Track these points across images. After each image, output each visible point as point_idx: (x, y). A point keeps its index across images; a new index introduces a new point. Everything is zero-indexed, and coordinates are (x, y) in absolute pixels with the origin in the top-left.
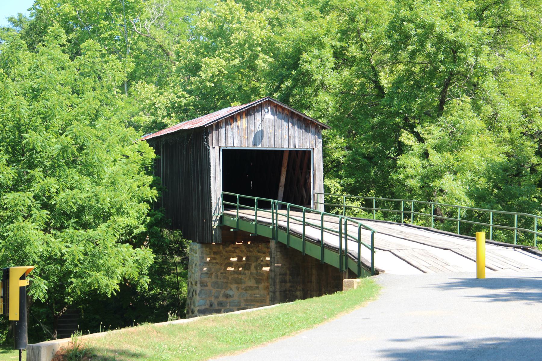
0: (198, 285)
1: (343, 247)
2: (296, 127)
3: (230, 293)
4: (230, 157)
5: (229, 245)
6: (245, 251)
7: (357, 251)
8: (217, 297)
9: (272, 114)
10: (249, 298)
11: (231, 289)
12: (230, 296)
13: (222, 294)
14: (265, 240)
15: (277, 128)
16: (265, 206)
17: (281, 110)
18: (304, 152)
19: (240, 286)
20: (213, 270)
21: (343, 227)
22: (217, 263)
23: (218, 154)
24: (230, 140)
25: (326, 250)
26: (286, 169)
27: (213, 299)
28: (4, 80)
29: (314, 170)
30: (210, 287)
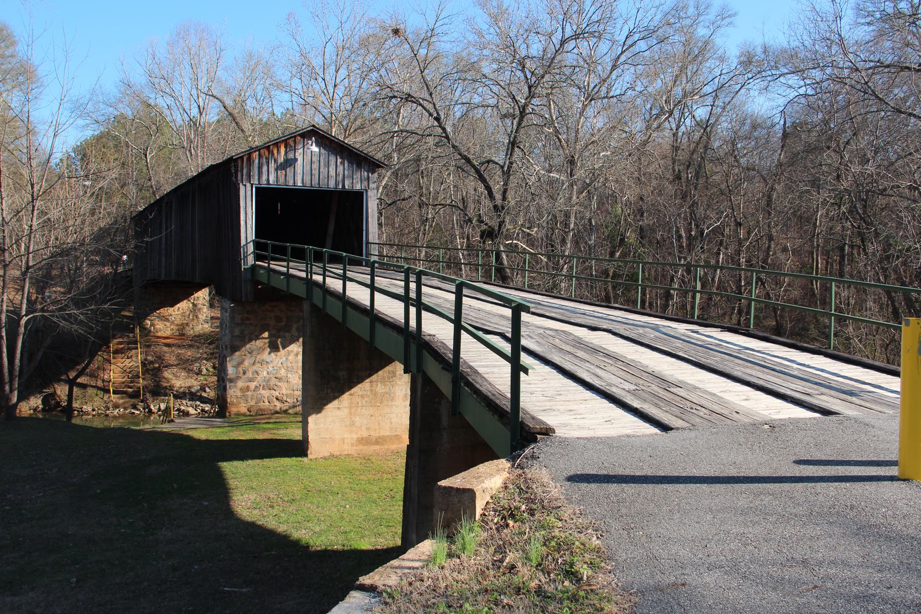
1: (413, 323)
2: (346, 163)
4: (267, 198)
7: (451, 344)
9: (317, 145)
14: (294, 299)
16: (299, 255)
17: (328, 143)
20: (246, 333)
21: (413, 286)
22: (251, 324)
23: (249, 193)
24: (264, 177)
25: (378, 326)
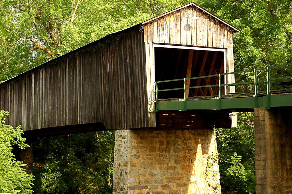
0: (129, 166)
3: (155, 172)
4: (163, 55)
5: (153, 131)
6: (166, 136)
8: (144, 176)
10: (170, 176)
11: (155, 169)
12: (155, 174)
13: (148, 173)
15: (198, 29)
18: (211, 54)
19: (162, 166)
26: (191, 71)
27: (141, 177)
28: (161, 179)
29: (227, 66)
30: (138, 167)
